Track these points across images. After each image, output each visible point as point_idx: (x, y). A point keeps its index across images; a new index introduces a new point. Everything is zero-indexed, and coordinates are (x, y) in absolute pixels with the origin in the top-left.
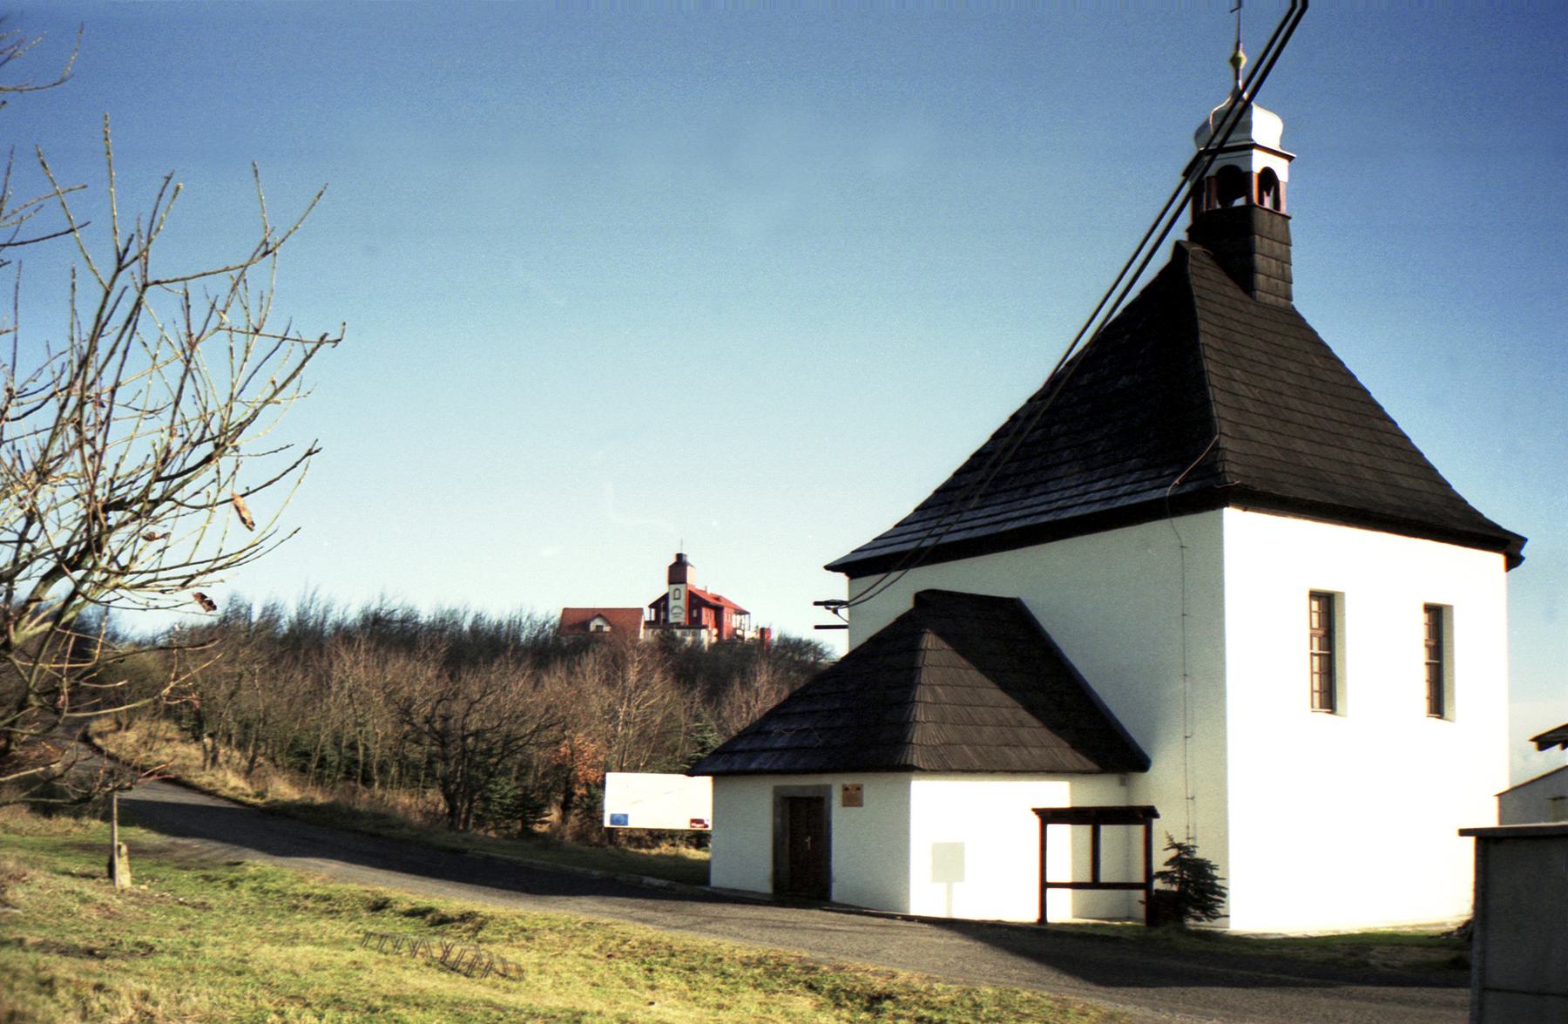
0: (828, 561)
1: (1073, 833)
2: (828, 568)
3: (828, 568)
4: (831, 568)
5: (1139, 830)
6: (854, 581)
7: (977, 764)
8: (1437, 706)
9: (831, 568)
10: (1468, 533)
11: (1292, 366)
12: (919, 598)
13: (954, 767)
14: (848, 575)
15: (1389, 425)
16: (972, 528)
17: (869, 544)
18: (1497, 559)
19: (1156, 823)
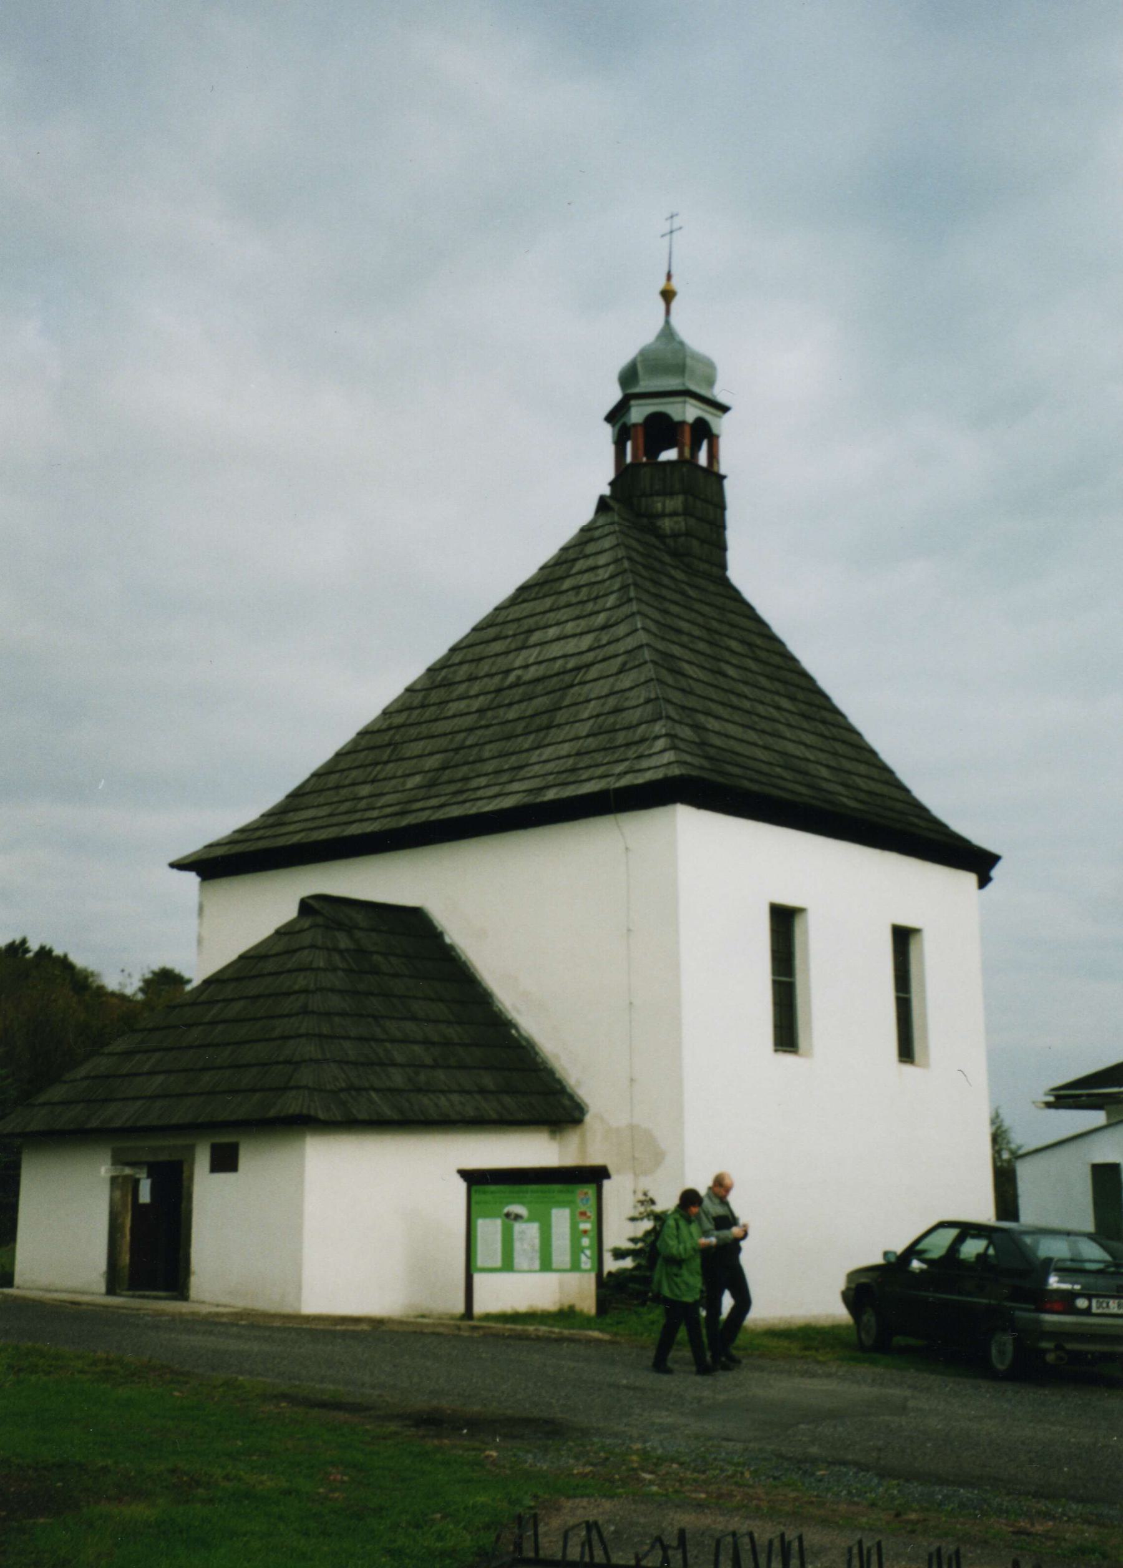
0: (175, 856)
1: (298, 1298)
2: (173, 865)
3: (173, 865)
4: (180, 865)
5: (590, 1190)
6: (206, 883)
7: (389, 1113)
8: (906, 1051)
9: (180, 865)
10: (603, 794)
11: (734, 645)
12: (307, 906)
13: (361, 1117)
14: (199, 874)
15: (840, 718)
16: (314, 819)
17: (229, 836)
18: (971, 879)
19: (607, 1184)
